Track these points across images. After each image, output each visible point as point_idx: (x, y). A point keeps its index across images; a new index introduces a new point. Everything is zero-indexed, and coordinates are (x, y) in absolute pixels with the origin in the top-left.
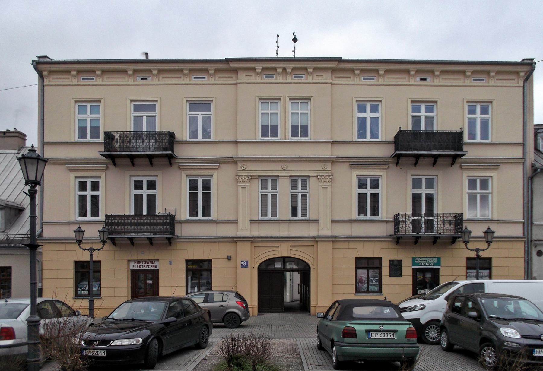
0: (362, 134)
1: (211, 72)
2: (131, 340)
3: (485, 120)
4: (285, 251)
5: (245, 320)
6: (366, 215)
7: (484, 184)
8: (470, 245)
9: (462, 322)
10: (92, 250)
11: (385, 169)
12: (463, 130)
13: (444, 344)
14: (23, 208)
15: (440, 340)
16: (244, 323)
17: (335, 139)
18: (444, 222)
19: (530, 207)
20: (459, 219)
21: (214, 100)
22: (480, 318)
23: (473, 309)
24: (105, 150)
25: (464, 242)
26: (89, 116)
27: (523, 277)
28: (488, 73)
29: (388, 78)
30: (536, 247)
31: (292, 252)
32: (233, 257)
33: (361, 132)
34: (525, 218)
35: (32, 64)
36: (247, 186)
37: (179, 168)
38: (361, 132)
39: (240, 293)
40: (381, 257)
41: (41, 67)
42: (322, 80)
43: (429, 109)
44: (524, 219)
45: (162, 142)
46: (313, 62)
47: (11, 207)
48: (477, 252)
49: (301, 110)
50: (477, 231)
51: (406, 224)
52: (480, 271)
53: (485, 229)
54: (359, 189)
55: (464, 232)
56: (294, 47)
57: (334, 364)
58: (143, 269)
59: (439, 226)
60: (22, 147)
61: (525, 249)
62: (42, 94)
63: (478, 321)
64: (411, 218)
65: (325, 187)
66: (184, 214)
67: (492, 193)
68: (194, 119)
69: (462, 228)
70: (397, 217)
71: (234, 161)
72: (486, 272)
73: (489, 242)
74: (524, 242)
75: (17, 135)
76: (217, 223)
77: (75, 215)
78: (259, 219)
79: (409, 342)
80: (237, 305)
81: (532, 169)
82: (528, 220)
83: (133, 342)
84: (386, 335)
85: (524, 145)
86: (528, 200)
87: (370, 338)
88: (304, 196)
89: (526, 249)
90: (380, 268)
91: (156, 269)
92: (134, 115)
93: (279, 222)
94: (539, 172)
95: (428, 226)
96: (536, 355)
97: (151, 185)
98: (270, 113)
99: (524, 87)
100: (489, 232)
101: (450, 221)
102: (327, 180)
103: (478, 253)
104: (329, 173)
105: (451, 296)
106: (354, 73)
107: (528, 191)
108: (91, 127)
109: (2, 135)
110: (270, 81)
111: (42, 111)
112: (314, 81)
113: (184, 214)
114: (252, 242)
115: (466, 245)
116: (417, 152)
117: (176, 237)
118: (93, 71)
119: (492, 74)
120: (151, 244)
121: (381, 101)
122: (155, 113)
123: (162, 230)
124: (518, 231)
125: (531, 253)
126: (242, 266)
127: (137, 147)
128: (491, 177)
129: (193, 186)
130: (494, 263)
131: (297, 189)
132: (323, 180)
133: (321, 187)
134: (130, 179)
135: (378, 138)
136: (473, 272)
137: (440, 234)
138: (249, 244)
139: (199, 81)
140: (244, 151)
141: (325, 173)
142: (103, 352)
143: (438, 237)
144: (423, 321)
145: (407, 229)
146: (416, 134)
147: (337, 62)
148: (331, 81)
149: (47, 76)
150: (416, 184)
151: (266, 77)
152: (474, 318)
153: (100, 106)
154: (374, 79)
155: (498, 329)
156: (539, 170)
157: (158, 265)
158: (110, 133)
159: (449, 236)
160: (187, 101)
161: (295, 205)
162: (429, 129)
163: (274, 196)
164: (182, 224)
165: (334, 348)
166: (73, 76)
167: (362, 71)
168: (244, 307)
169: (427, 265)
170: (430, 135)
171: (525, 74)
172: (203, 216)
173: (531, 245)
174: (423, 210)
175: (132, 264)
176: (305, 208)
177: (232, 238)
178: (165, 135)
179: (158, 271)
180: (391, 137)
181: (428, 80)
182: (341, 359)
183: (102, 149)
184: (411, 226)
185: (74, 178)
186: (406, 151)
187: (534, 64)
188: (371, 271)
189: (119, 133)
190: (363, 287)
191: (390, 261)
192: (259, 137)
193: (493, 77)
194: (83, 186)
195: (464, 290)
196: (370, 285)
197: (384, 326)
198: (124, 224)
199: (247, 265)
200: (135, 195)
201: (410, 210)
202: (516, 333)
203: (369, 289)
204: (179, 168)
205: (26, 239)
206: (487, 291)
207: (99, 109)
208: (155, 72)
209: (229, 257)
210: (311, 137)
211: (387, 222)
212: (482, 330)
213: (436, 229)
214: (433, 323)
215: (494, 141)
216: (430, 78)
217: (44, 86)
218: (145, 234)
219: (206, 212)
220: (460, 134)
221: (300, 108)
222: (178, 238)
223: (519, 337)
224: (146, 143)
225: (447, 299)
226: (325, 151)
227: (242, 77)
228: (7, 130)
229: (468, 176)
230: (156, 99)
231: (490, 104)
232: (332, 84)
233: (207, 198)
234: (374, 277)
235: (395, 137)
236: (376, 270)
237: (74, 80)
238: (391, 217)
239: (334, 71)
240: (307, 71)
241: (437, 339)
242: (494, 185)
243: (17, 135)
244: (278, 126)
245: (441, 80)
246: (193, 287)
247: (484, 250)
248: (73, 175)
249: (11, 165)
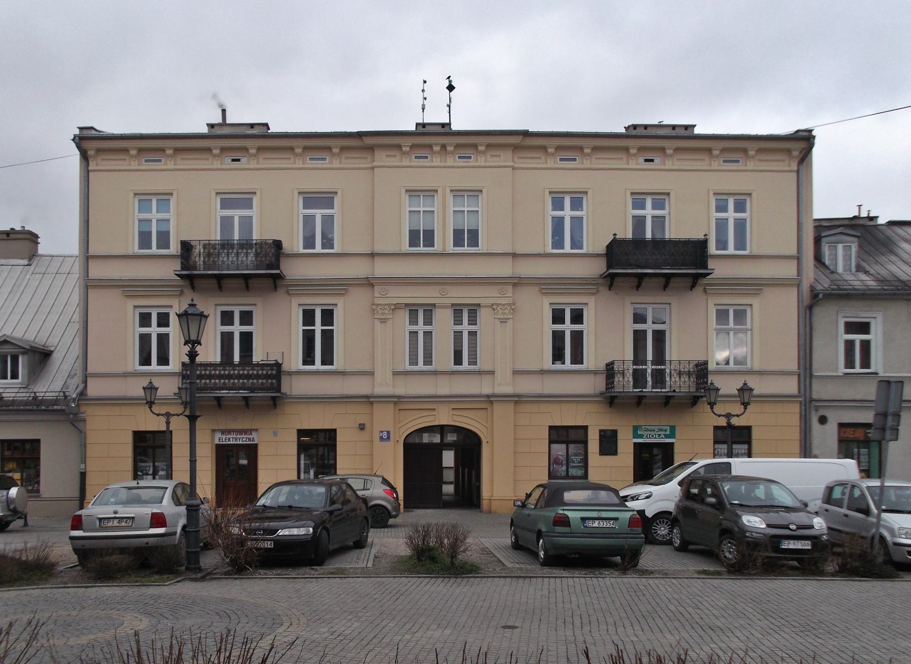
0: (558, 242)
1: (336, 150)
2: (301, 529)
3: (741, 221)
4: (444, 417)
5: (395, 517)
6: (564, 363)
8: (718, 409)
9: (699, 511)
10: (168, 415)
11: (593, 294)
12: (708, 237)
13: (677, 542)
14: (50, 351)
15: (671, 538)
16: (391, 521)
17: (520, 250)
18: (680, 374)
19: (808, 351)
20: (702, 369)
21: (339, 192)
22: (720, 506)
23: (712, 495)
24: (182, 268)
25: (709, 404)
26: (154, 215)
27: (798, 455)
28: (745, 151)
30: (817, 410)
31: (455, 418)
32: (368, 426)
33: (557, 238)
34: (801, 367)
35: (73, 140)
36: (388, 319)
38: (557, 238)
39: (386, 477)
40: (587, 426)
41: (86, 145)
42: (498, 161)
43: (658, 205)
44: (799, 369)
45: (266, 255)
46: (486, 137)
47: (35, 349)
49: (467, 206)
50: (728, 386)
51: (623, 377)
52: (734, 446)
53: (740, 386)
54: (554, 323)
55: (709, 389)
56: (450, 99)
57: (541, 560)
58: (234, 443)
59: (673, 379)
60: (34, 255)
61: (801, 413)
62: (86, 183)
63: (718, 509)
64: (631, 367)
65: (503, 321)
66: (294, 361)
67: (751, 330)
68: (309, 221)
69: (707, 383)
70: (610, 367)
71: (369, 283)
72: (742, 448)
73: (745, 405)
74: (800, 403)
75: (27, 236)
76: (344, 375)
77: (134, 363)
78: (406, 368)
79: (632, 532)
80: (384, 494)
81: (811, 295)
82: (805, 369)
83: (302, 531)
84: (605, 523)
85: (798, 259)
86: (806, 340)
87: (586, 527)
88: (473, 334)
89: (803, 413)
90: (585, 442)
91: (253, 442)
92: (220, 214)
93: (435, 373)
94: (820, 299)
95: (656, 379)
96: (783, 547)
97: (247, 318)
98: (422, 212)
99: (798, 171)
100: (745, 390)
101: (689, 371)
102: (507, 311)
103: (729, 420)
104: (510, 301)
105: (686, 479)
106: (547, 151)
107: (805, 327)
108: (158, 233)
109: (5, 236)
110: (421, 164)
111: (86, 209)
112: (488, 164)
113: (294, 361)
114: (395, 403)
115: (712, 408)
116: (640, 271)
117: (284, 396)
118: (163, 150)
119: (751, 153)
120: (247, 405)
121: (586, 193)
122: (252, 211)
123: (265, 385)
124: (790, 386)
125: (810, 419)
126: (381, 438)
127: (230, 263)
128: (751, 305)
129: (309, 318)
130: (755, 434)
131: (462, 324)
132: (500, 312)
133: (497, 322)
134: (215, 310)
135: (581, 248)
136: (723, 448)
137: (674, 391)
138: (392, 405)
139: (316, 164)
140: (384, 269)
141: (503, 301)
142: (269, 543)
143: (670, 397)
144: (649, 514)
145: (625, 384)
146: (638, 243)
147: (522, 137)
148: (512, 164)
149: (94, 157)
150: (639, 318)
151: (416, 157)
152: (712, 505)
153: (171, 200)
154: (576, 161)
155: (739, 517)
156: (821, 296)
157: (255, 438)
158: (189, 243)
159: (687, 394)
160: (300, 193)
161: (458, 349)
162: (658, 236)
163: (428, 334)
164: (293, 376)
165: (541, 541)
166: (132, 156)
167: (559, 148)
168: (394, 498)
169: (655, 438)
170: (659, 244)
171: (800, 152)
172: (323, 363)
173: (810, 407)
174: (650, 357)
175: (218, 435)
176: (473, 353)
177: (367, 397)
178: (269, 245)
179: (256, 446)
180: (601, 248)
181: (655, 161)
182: (550, 553)
183: (177, 265)
184: (631, 379)
185: (132, 307)
186: (623, 269)
187: (812, 139)
188: (571, 446)
189: (202, 243)
190: (560, 470)
191: (601, 431)
192: (406, 247)
193: (753, 157)
194: (145, 320)
195: (705, 472)
196: (571, 468)
197: (602, 513)
198: (210, 377)
199: (388, 438)
200: (222, 333)
201: (630, 356)
202: (760, 521)
203: (570, 473)
204: (288, 292)
205: (61, 399)
206: (734, 473)
207: (169, 205)
208: (253, 151)
209: (363, 426)
210: (482, 247)
211: (595, 374)
212: (722, 519)
213: (668, 384)
214: (662, 515)
215: (756, 252)
216: (659, 158)
217: (88, 171)
218: (240, 391)
219: (327, 358)
220: (703, 244)
221: (466, 203)
222: (287, 398)
223: (764, 526)
224: (242, 257)
225: (680, 484)
226: (504, 269)
227: (382, 158)
228: (11, 229)
229: (715, 305)
231: (748, 196)
232: (513, 168)
233: (328, 337)
234: (576, 455)
235: (607, 246)
236: (579, 445)
237: (132, 163)
238: (602, 366)
239: (516, 148)
240: (477, 149)
241: (668, 538)
242: (754, 317)
243: (27, 236)
244: (434, 230)
245: (261, 160)
246: (307, 472)
247: (738, 416)
248: (131, 303)
249: (21, 283)
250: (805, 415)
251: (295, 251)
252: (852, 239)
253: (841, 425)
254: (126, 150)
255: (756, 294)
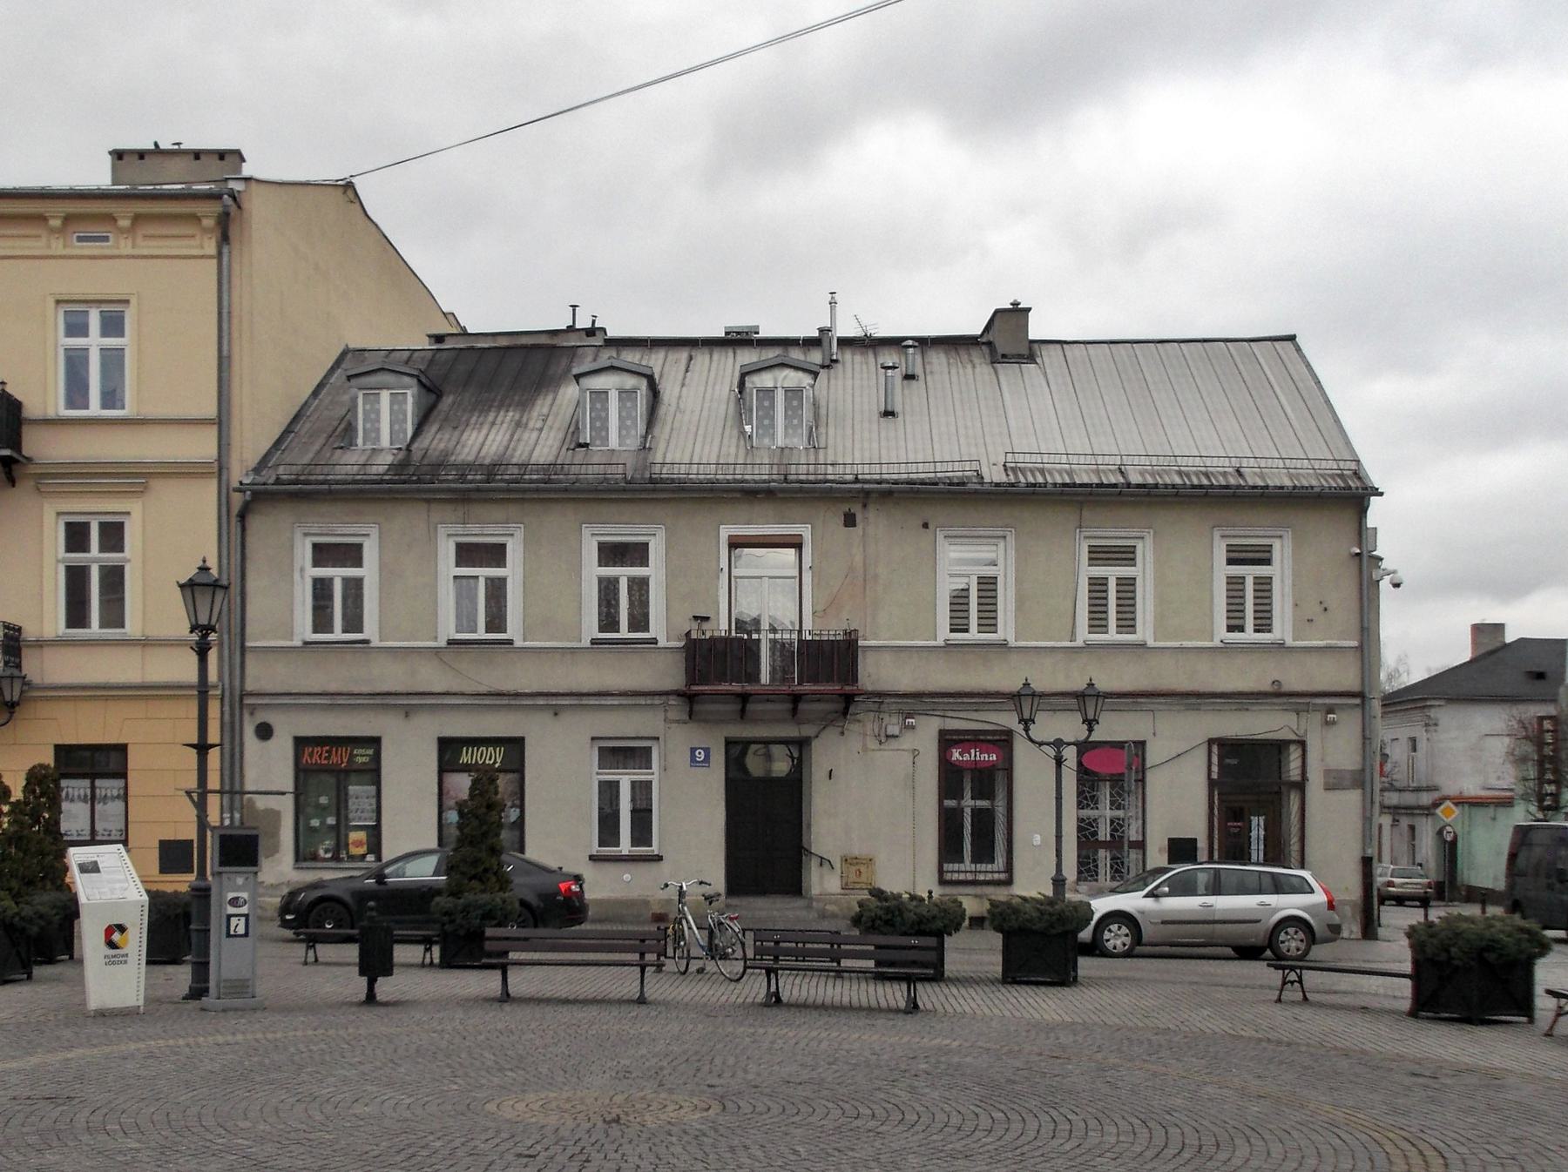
7: (113, 535)
29: (145, 236)
30: (252, 714)
37: (38, 489)
48: (1058, 749)
66: (51, 619)
89: (227, 717)
185: (54, 515)
204: (38, 489)
219: (114, 614)
230: (124, 297)
245: (139, 241)
250: (232, 723)
251: (51, 414)
252: (407, 379)
253: (301, 743)
254: (41, 219)
255: (140, 491)
